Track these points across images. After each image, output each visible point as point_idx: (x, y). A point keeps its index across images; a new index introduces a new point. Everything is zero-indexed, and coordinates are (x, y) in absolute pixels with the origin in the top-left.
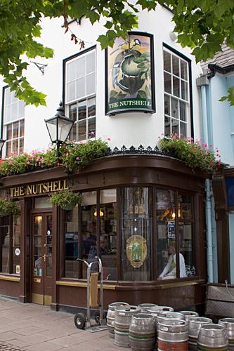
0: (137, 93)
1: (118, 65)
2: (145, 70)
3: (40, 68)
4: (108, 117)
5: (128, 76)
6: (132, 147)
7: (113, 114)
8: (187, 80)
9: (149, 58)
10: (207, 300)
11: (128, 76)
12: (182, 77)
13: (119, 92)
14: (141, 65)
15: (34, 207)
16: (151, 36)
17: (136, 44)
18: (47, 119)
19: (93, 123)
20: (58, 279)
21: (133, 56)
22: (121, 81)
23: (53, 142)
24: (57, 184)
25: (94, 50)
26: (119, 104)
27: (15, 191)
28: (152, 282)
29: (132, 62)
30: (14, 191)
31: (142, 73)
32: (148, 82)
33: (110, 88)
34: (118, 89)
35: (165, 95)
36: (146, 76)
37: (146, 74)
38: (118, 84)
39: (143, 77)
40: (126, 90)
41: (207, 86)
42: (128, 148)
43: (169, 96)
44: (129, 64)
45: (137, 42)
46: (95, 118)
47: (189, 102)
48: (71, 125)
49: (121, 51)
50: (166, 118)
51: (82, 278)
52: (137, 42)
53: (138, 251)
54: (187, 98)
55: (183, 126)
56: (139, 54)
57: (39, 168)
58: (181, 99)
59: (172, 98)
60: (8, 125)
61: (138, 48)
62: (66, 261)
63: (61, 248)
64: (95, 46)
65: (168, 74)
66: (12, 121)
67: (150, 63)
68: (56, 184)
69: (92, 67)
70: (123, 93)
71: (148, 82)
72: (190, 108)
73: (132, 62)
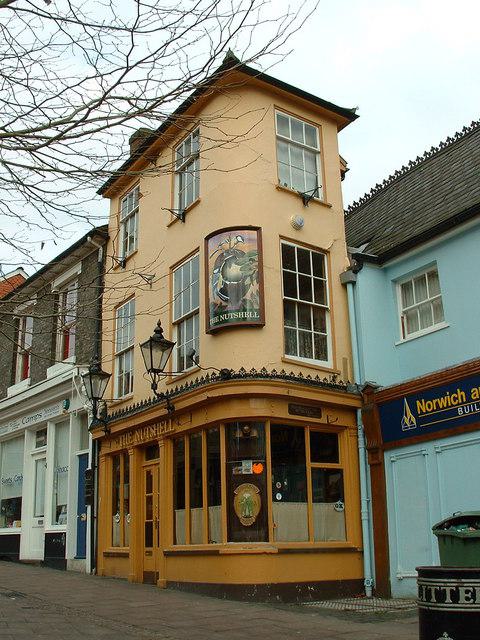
9: (256, 258)
16: (257, 229)
21: (234, 257)
23: (149, 371)
31: (246, 277)
33: (211, 300)
36: (252, 281)
39: (248, 281)
41: (354, 283)
50: (286, 331)
52: (239, 239)
53: (248, 503)
57: (127, 413)
59: (299, 303)
63: (364, 516)
64: (133, 347)
69: (196, 267)
71: (254, 288)
73: (233, 265)
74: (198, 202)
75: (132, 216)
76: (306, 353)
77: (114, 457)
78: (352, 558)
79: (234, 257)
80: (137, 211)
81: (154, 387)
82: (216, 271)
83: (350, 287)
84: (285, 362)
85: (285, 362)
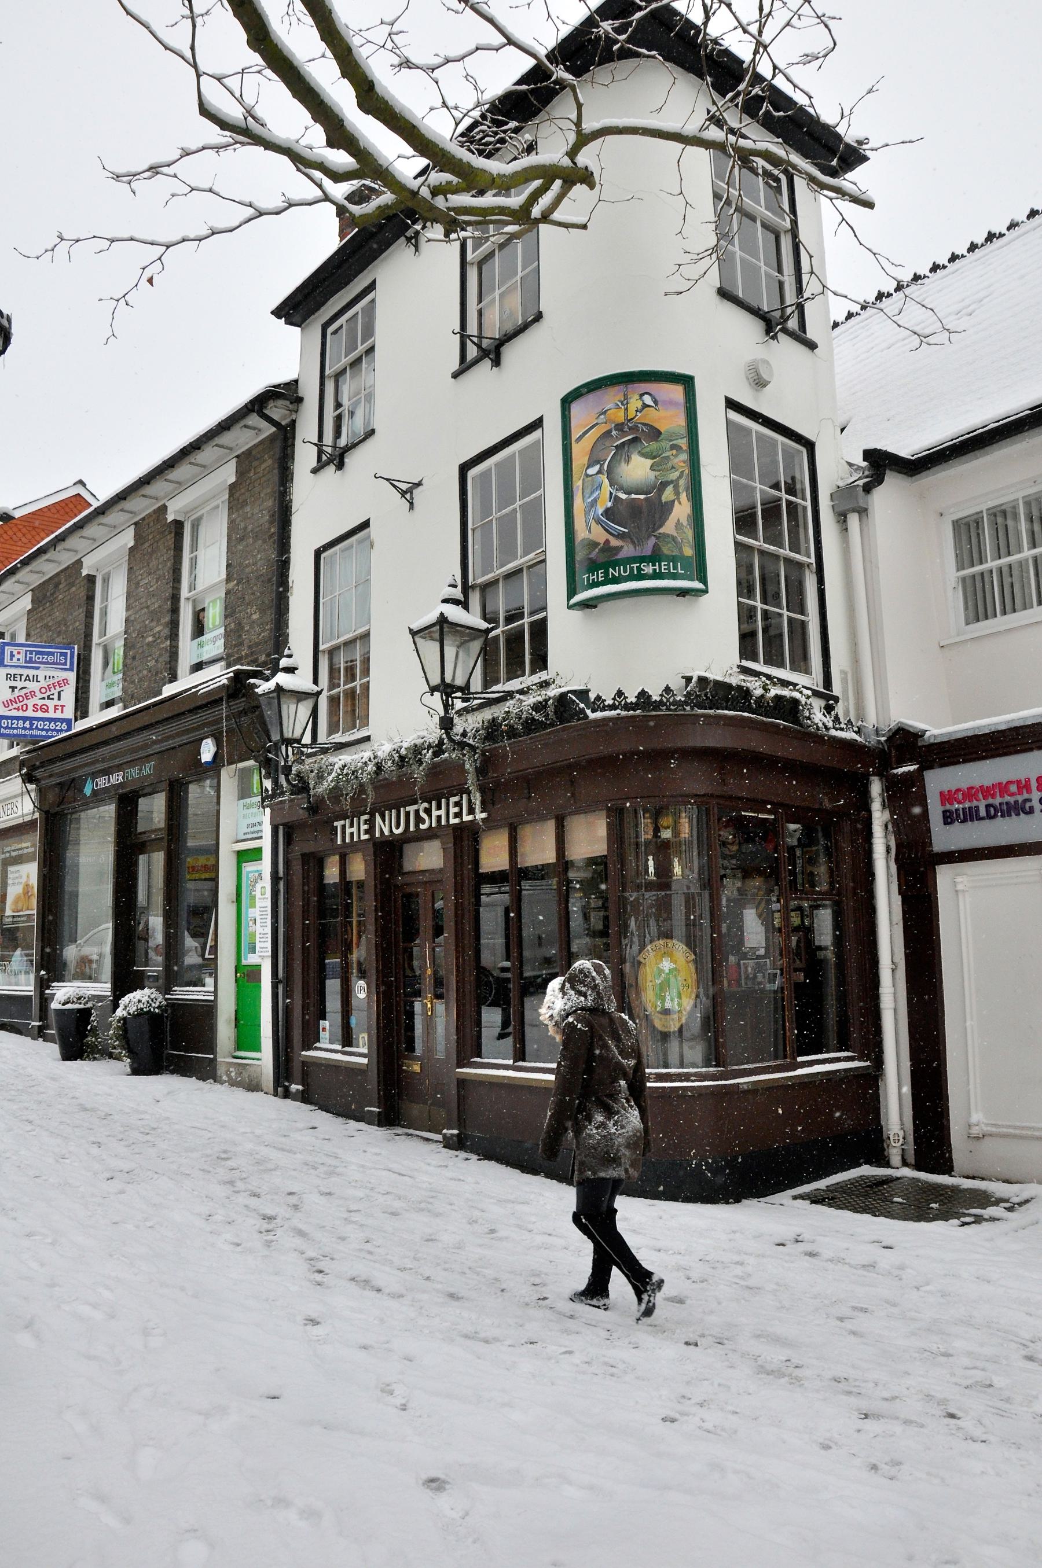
0: (652, 541)
1: (597, 468)
2: (674, 475)
3: (403, 493)
4: (577, 614)
5: (623, 496)
6: (643, 694)
7: (587, 605)
8: (804, 499)
9: (683, 443)
11: (623, 496)
13: (602, 541)
14: (659, 462)
15: (401, 866)
16: (687, 382)
17: (645, 406)
18: (415, 626)
19: (540, 630)
20: (460, 1066)
21: (635, 440)
22: (607, 512)
24: (458, 804)
25: (536, 435)
26: (606, 573)
27: (348, 831)
28: (779, 1062)
30: (344, 827)
31: (664, 485)
32: (682, 510)
33: (581, 533)
34: (599, 535)
35: (738, 544)
36: (677, 493)
38: (598, 522)
39: (668, 494)
40: (621, 536)
41: (863, 512)
42: (632, 699)
43: (749, 548)
44: (628, 462)
45: (648, 400)
47: (813, 560)
48: (482, 640)
49: (604, 428)
51: (350, 1045)
52: (648, 400)
54: (808, 549)
55: (799, 630)
56: (655, 434)
58: (786, 552)
60: (332, 652)
61: (652, 416)
62: (212, 998)
65: (746, 486)
66: (341, 639)
67: (684, 456)
68: (458, 804)
71: (682, 510)
74: (539, 317)
75: (356, 363)
76: (774, 658)
77: (306, 857)
78: (678, 1063)
79: (635, 440)
80: (371, 350)
81: (446, 723)
82: (592, 471)
83: (853, 520)
84: (745, 670)
85: (745, 670)
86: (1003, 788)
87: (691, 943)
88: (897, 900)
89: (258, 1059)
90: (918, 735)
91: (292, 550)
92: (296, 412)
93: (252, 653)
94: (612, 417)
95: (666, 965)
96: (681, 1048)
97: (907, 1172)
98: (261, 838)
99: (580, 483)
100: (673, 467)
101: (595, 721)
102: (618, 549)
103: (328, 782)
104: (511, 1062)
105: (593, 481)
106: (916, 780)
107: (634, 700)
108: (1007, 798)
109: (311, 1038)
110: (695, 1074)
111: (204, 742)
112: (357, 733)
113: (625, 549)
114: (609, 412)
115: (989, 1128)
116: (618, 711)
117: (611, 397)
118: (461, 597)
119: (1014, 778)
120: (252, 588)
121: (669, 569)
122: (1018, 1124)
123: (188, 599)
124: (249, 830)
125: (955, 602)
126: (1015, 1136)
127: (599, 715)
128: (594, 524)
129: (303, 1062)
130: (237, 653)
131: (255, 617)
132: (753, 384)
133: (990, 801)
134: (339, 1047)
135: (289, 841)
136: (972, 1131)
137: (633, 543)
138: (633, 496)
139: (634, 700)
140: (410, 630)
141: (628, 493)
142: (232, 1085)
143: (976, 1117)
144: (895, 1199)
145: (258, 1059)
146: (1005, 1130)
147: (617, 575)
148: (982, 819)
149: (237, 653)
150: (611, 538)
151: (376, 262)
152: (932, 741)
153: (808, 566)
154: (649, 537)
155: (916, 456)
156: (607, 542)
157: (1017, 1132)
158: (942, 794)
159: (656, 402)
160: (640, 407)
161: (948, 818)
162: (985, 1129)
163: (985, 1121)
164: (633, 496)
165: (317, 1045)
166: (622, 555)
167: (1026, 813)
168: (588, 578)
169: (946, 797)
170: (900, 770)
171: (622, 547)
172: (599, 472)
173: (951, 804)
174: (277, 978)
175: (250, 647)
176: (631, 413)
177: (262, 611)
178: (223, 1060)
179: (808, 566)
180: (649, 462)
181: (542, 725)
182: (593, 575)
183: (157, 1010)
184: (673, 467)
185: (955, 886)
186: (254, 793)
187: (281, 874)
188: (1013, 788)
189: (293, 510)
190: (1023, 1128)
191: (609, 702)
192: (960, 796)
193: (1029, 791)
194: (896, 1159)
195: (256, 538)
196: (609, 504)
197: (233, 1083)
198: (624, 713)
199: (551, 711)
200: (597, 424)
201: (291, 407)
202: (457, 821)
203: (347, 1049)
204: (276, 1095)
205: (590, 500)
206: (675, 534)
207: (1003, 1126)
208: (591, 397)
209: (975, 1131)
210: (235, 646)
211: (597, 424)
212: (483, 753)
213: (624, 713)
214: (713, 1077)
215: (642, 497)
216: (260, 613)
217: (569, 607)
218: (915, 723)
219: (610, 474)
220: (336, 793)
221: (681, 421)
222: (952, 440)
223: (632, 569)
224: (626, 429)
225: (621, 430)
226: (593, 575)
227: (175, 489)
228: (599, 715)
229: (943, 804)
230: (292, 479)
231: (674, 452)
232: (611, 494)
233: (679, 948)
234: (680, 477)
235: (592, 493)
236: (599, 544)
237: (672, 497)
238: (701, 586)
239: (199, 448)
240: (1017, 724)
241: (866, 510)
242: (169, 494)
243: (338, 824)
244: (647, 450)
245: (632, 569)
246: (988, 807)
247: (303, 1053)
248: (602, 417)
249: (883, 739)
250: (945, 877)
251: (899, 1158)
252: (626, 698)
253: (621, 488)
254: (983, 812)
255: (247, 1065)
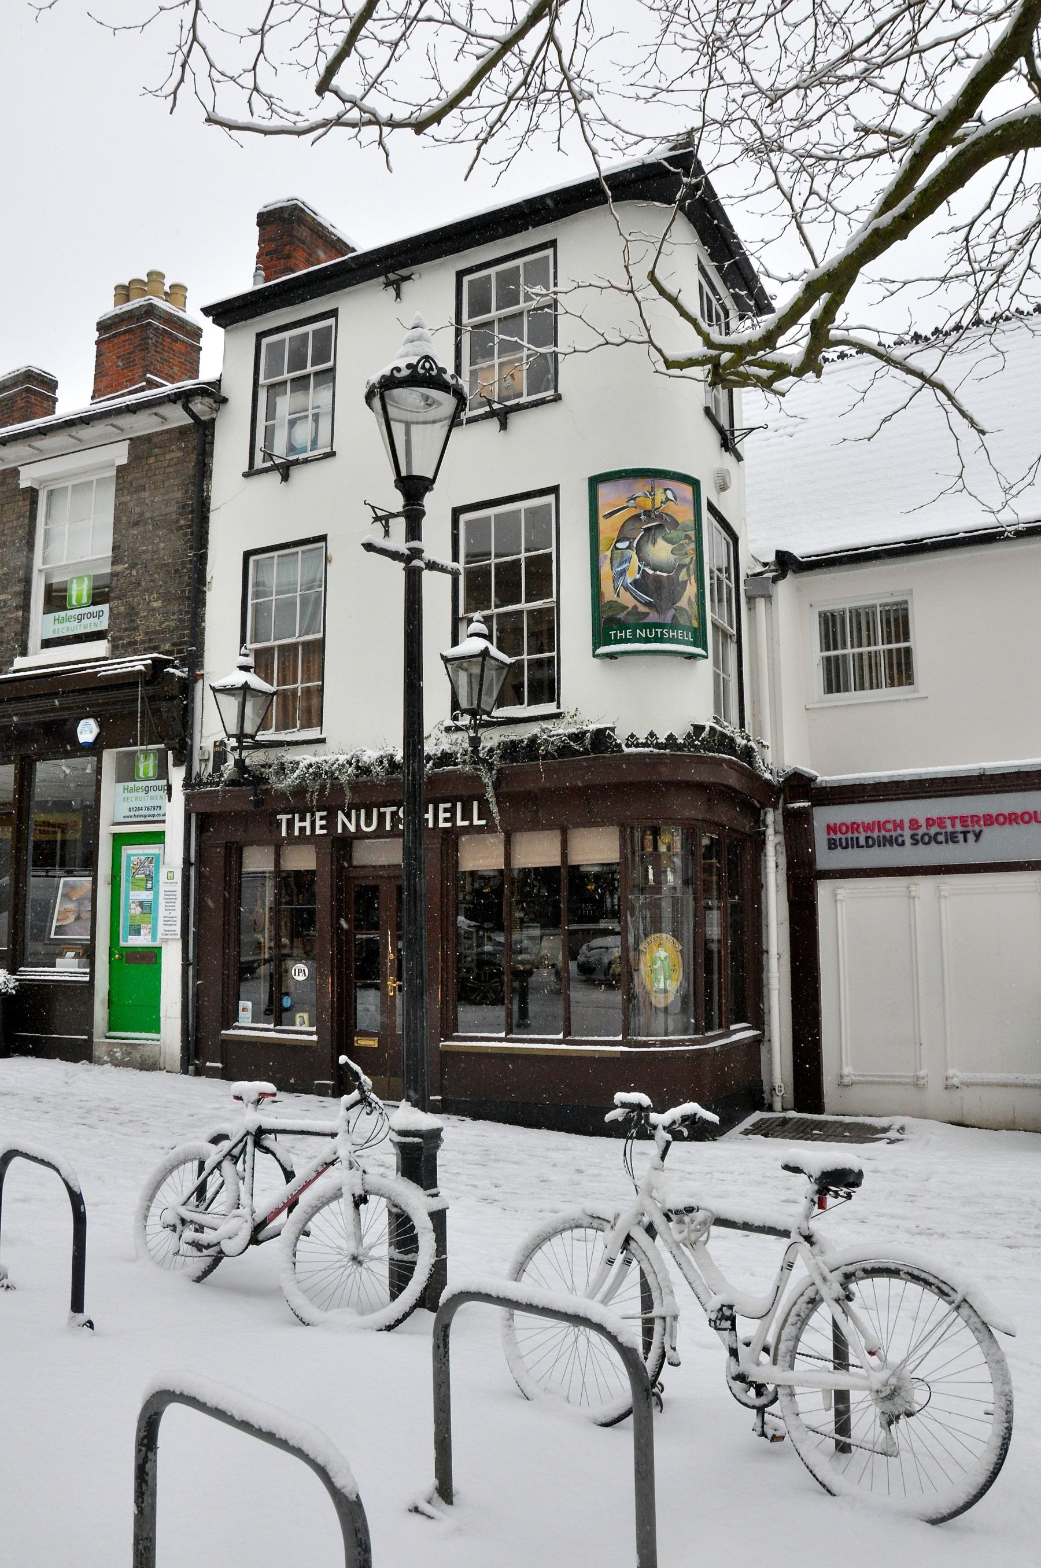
2: (687, 560)
5: (651, 572)
6: (671, 737)
9: (692, 534)
10: (849, 1365)
11: (651, 572)
12: (719, 675)
17: (668, 499)
21: (660, 527)
22: (635, 583)
24: (452, 810)
26: (634, 634)
29: (660, 541)
31: (681, 566)
36: (689, 575)
37: (688, 570)
38: (626, 589)
39: (683, 576)
40: (647, 604)
41: (769, 598)
42: (662, 740)
44: (654, 543)
45: (669, 494)
46: (908, 651)
47: (735, 632)
52: (669, 494)
56: (675, 524)
67: (693, 546)
70: (642, 609)
72: (293, 749)
82: (620, 545)
86: (881, 825)
87: (676, 935)
88: (785, 906)
89: (158, 1040)
90: (812, 779)
91: (209, 546)
92: (217, 411)
93: (150, 640)
94: (642, 504)
95: (662, 954)
96: (666, 1020)
97: (792, 1114)
98: (164, 822)
99: (609, 553)
100: (686, 554)
101: (629, 755)
102: (647, 614)
103: (291, 779)
104: (503, 1035)
105: (622, 554)
106: (804, 816)
107: (664, 741)
108: (883, 833)
109: (230, 1017)
110: (689, 1040)
111: (82, 722)
112: (297, 733)
113: (651, 615)
114: (638, 499)
115: (858, 1078)
116: (651, 749)
117: (640, 488)
118: (486, 632)
119: (892, 818)
120: (152, 575)
121: (683, 636)
122: (882, 1074)
123: (40, 571)
124: (132, 813)
125: (817, 676)
126: (879, 1083)
127: (633, 750)
128: (622, 591)
129: (222, 1041)
130: (129, 636)
131: (155, 604)
132: (718, 488)
133: (869, 834)
134: (271, 1026)
135: (201, 829)
136: (843, 1081)
137: (657, 611)
138: (658, 573)
139: (664, 741)
140: (442, 656)
141: (655, 570)
142: (116, 1065)
143: (847, 1070)
144: (814, 1132)
145: (158, 1040)
146: (870, 1079)
147: (644, 636)
148: (862, 847)
149: (129, 636)
150: (638, 604)
151: (339, 293)
152: (824, 785)
153: (730, 636)
154: (670, 609)
155: (805, 559)
156: (635, 607)
157: (882, 1079)
158: (828, 826)
159: (675, 498)
160: (664, 500)
161: (832, 845)
162: (854, 1078)
163: (853, 1072)
164: (658, 573)
165: (236, 1024)
166: (647, 620)
167: (898, 845)
168: (615, 635)
169: (830, 829)
170: (796, 805)
171: (648, 614)
172: (629, 547)
173: (835, 833)
174: (188, 961)
175: (147, 633)
176: (657, 504)
177: (167, 598)
178: (98, 1040)
179: (730, 636)
180: (670, 547)
181: (576, 753)
182: (621, 632)
183: (14, 992)
184: (686, 554)
185: (836, 896)
186: (138, 776)
187: (193, 860)
188: (890, 826)
189: (212, 507)
190: (887, 1076)
191: (642, 740)
192: (844, 829)
193: (902, 829)
194: (778, 1105)
195: (157, 527)
196: (638, 576)
197: (117, 1063)
198: (656, 751)
199: (587, 741)
200: (627, 507)
201: (214, 405)
202: (449, 825)
203: (278, 1027)
204: (185, 1072)
205: (619, 569)
206: (687, 609)
207: (868, 1076)
208: (621, 483)
209: (846, 1080)
210: (126, 630)
211: (627, 507)
212: (499, 771)
213: (656, 751)
214: (694, 1042)
215: (665, 574)
216: (163, 601)
217: (594, 656)
218: (808, 769)
219: (639, 550)
220: (300, 791)
221: (690, 516)
222: (840, 552)
223: (656, 632)
224: (653, 516)
225: (649, 516)
226: (621, 632)
227: (36, 455)
228: (633, 750)
229: (828, 833)
230: (211, 476)
231: (687, 541)
232: (639, 568)
233: (666, 937)
234: (690, 563)
235: (621, 564)
236: (628, 608)
237: (686, 578)
238: (703, 653)
239: (88, 424)
240: (895, 779)
241: (770, 597)
242: (23, 459)
243: (284, 818)
244: (669, 536)
245: (656, 632)
246: (867, 838)
247: (223, 1032)
248: (632, 501)
249: (781, 780)
250: (824, 890)
251: (780, 1104)
252: (657, 738)
253: (647, 565)
254: (862, 842)
255: (140, 1045)
